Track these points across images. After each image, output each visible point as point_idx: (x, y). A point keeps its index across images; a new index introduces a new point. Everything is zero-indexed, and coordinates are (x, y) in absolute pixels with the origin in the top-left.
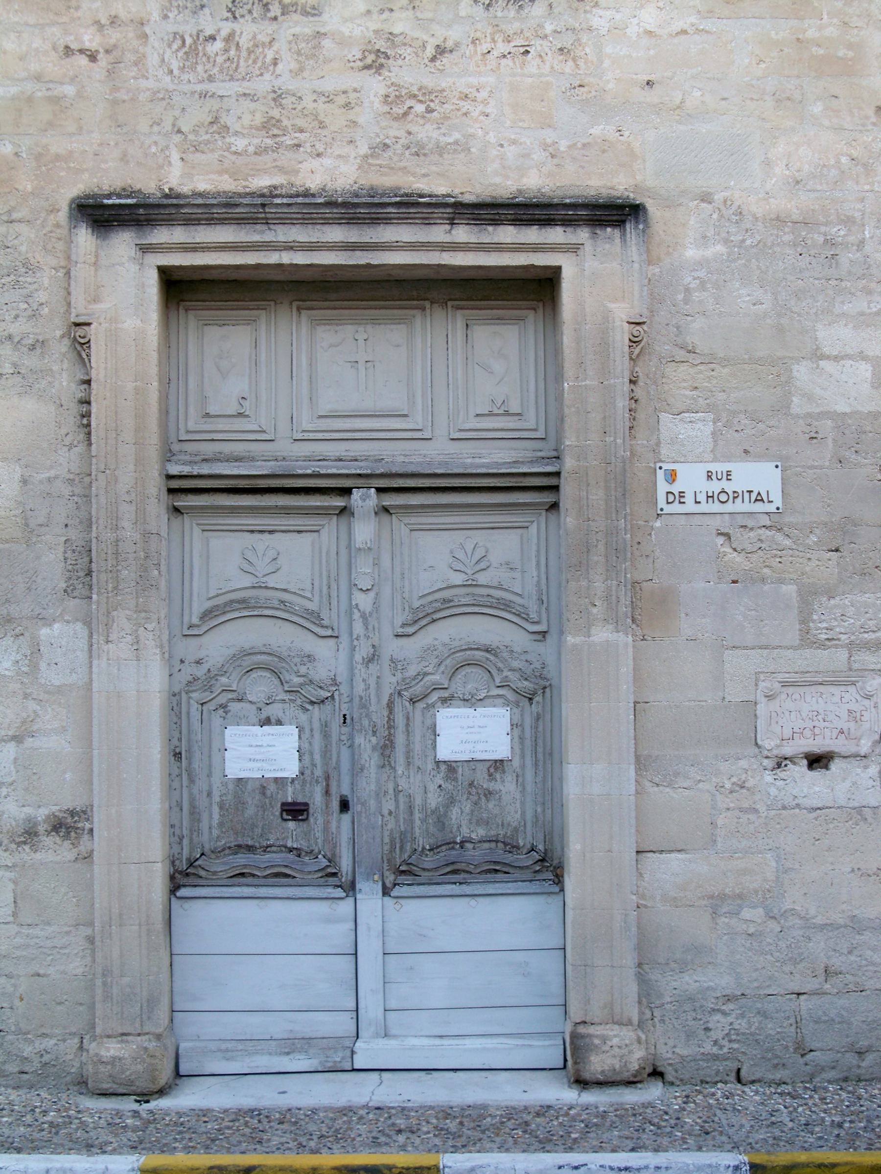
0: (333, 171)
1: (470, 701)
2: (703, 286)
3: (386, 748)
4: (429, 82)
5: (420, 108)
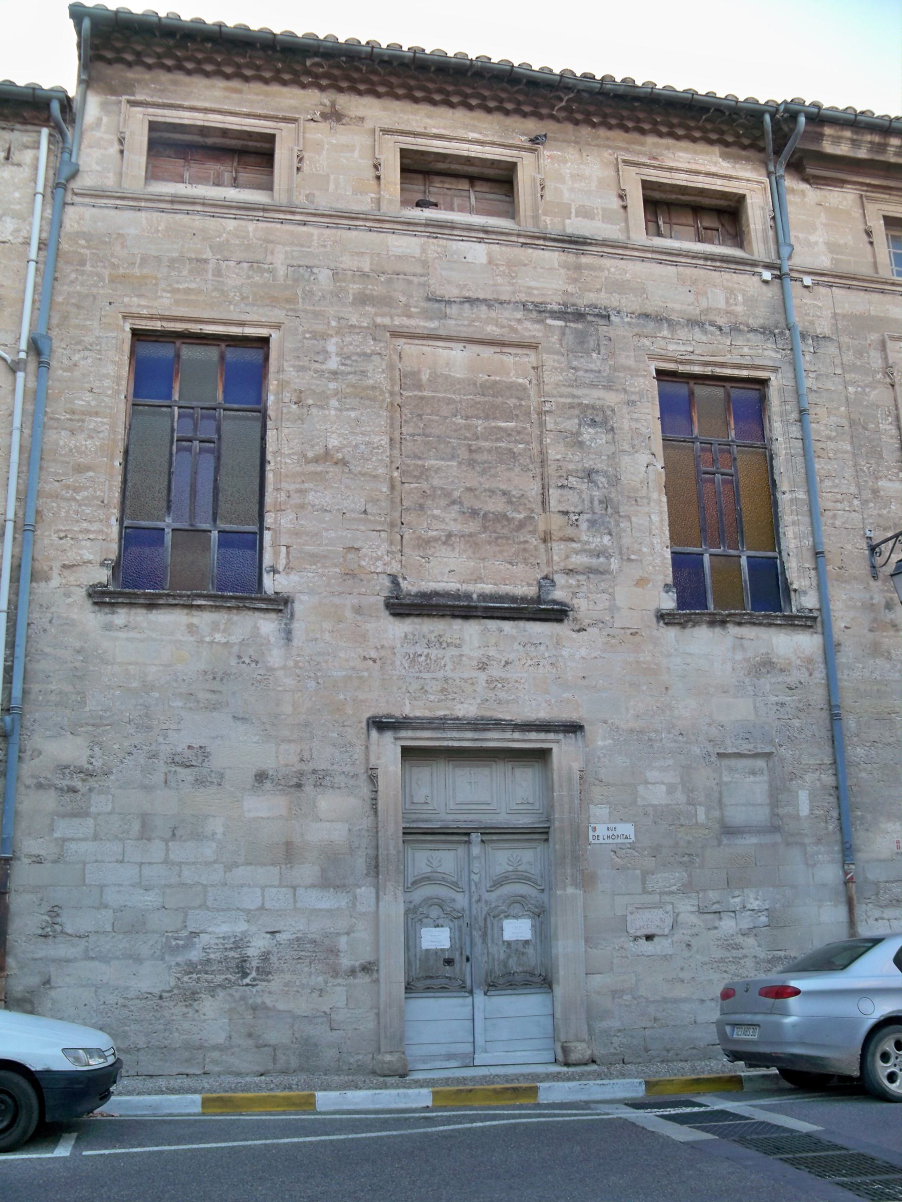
0: (467, 709)
1: (516, 917)
2: (605, 756)
3: (484, 935)
4: (503, 675)
5: (500, 685)
